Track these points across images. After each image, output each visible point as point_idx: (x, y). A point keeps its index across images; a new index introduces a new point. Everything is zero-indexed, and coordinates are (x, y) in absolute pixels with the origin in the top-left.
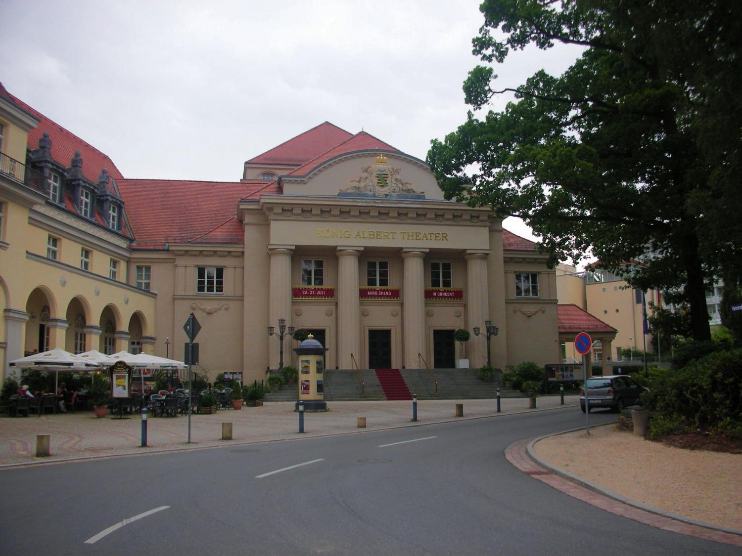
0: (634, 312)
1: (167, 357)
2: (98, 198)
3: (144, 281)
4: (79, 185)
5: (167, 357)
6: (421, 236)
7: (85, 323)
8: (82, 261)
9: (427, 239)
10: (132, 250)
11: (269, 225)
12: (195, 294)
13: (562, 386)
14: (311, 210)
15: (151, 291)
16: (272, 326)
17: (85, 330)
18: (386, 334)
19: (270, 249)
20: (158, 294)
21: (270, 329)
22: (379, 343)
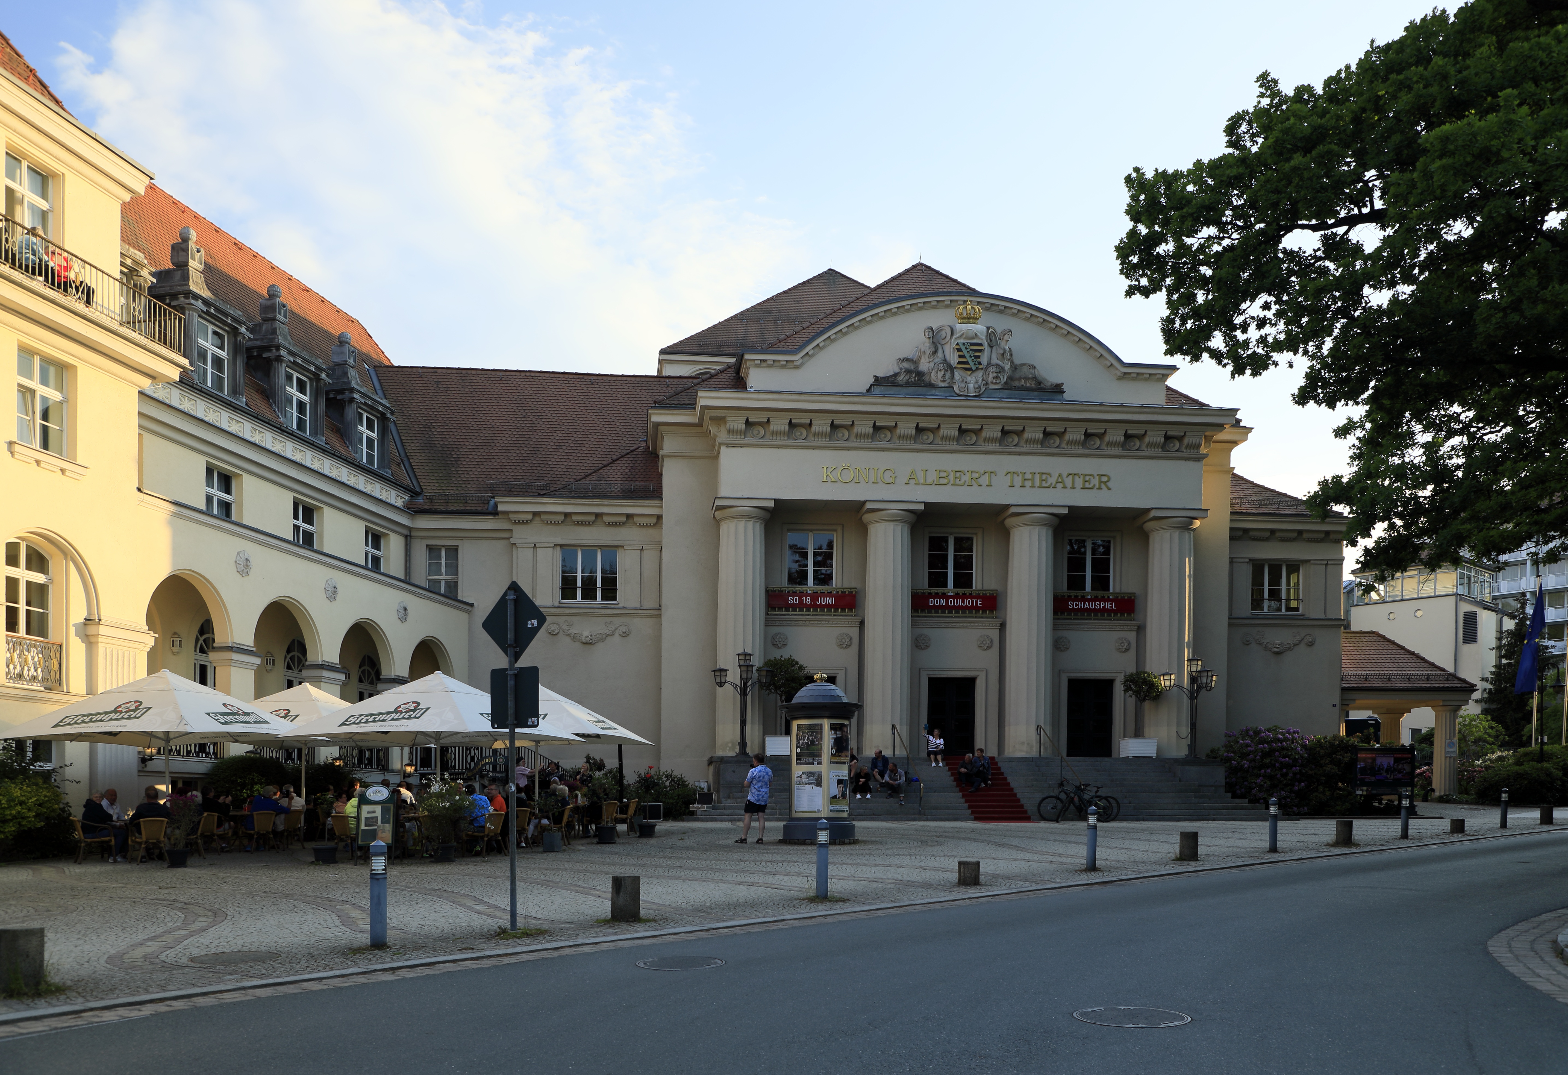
0: (1456, 660)
1: (620, 747)
2: (331, 396)
3: (444, 578)
4: (279, 359)
5: (620, 747)
6: (1052, 480)
7: (378, 673)
8: (367, 555)
9: (1065, 487)
10: (413, 510)
11: (716, 457)
12: (557, 604)
13: (1506, 792)
14: (810, 424)
15: (460, 598)
16: (723, 667)
17: (213, 656)
18: (964, 688)
19: (719, 508)
20: (476, 605)
21: (718, 673)
22: (949, 704)
